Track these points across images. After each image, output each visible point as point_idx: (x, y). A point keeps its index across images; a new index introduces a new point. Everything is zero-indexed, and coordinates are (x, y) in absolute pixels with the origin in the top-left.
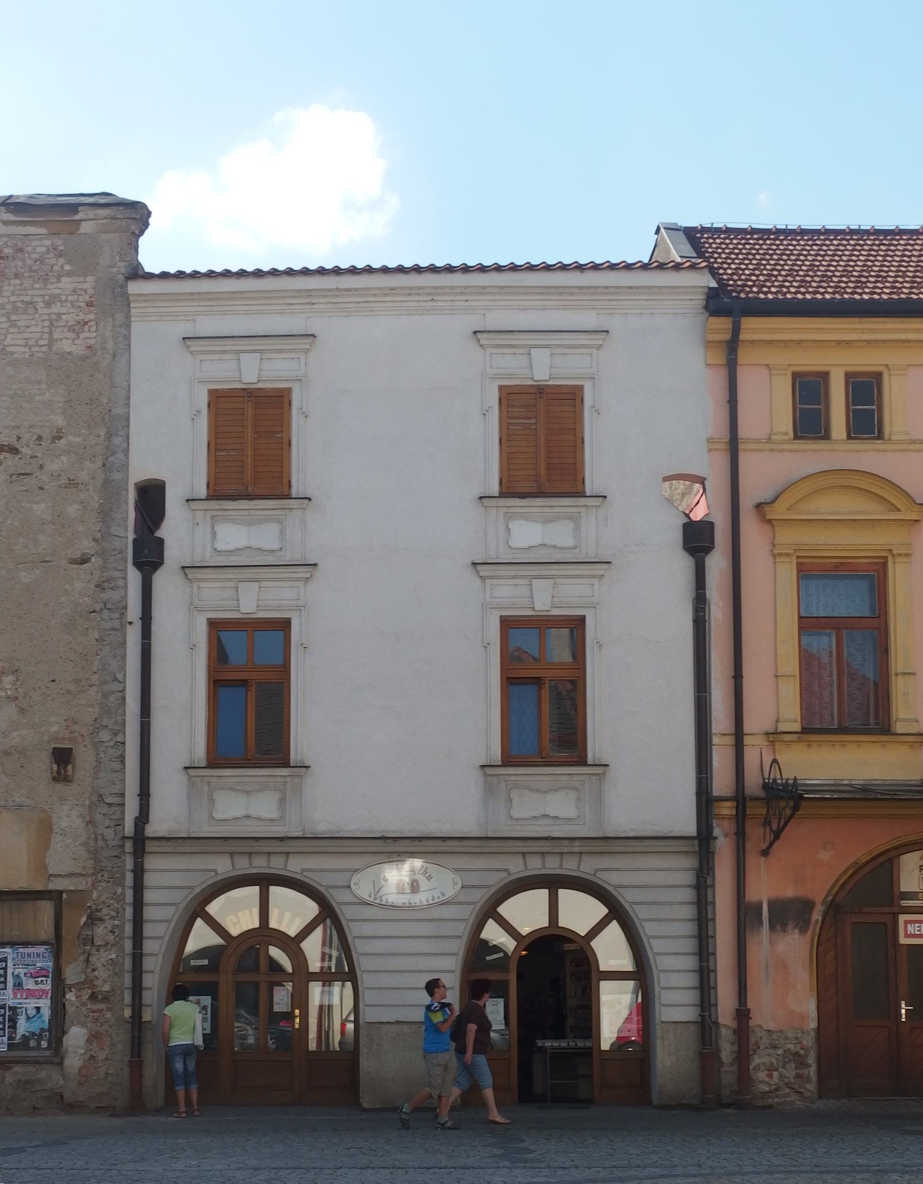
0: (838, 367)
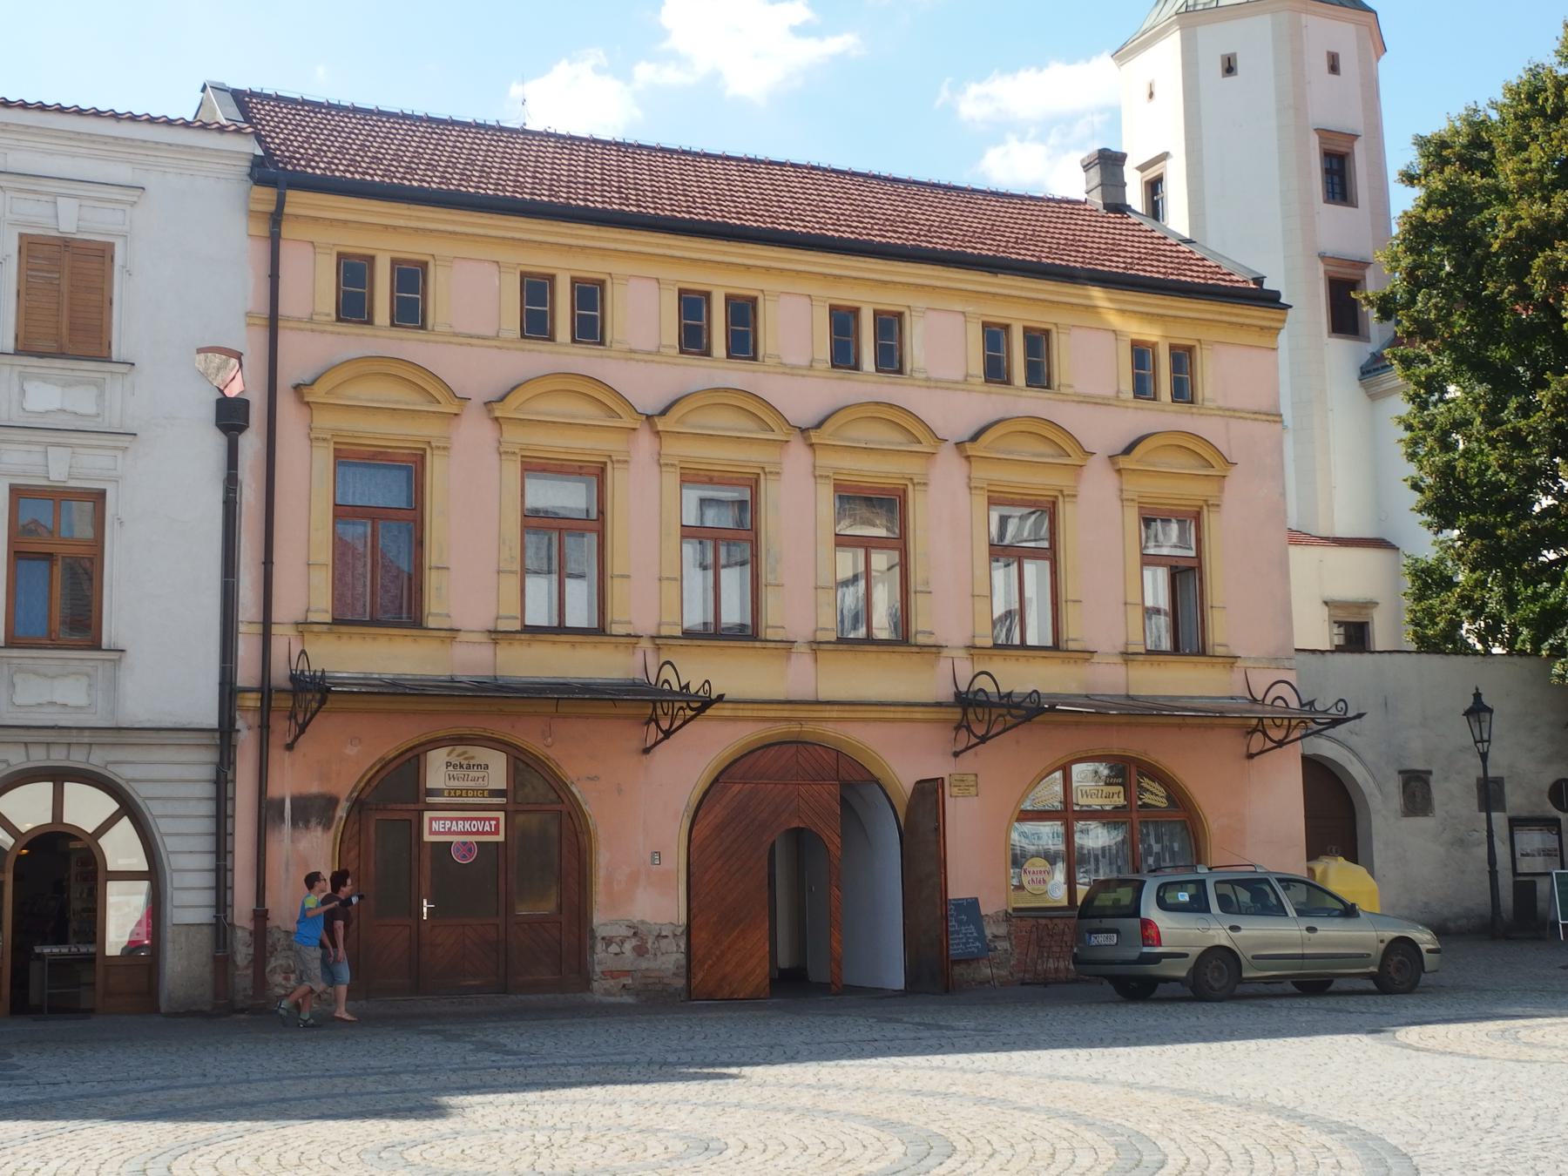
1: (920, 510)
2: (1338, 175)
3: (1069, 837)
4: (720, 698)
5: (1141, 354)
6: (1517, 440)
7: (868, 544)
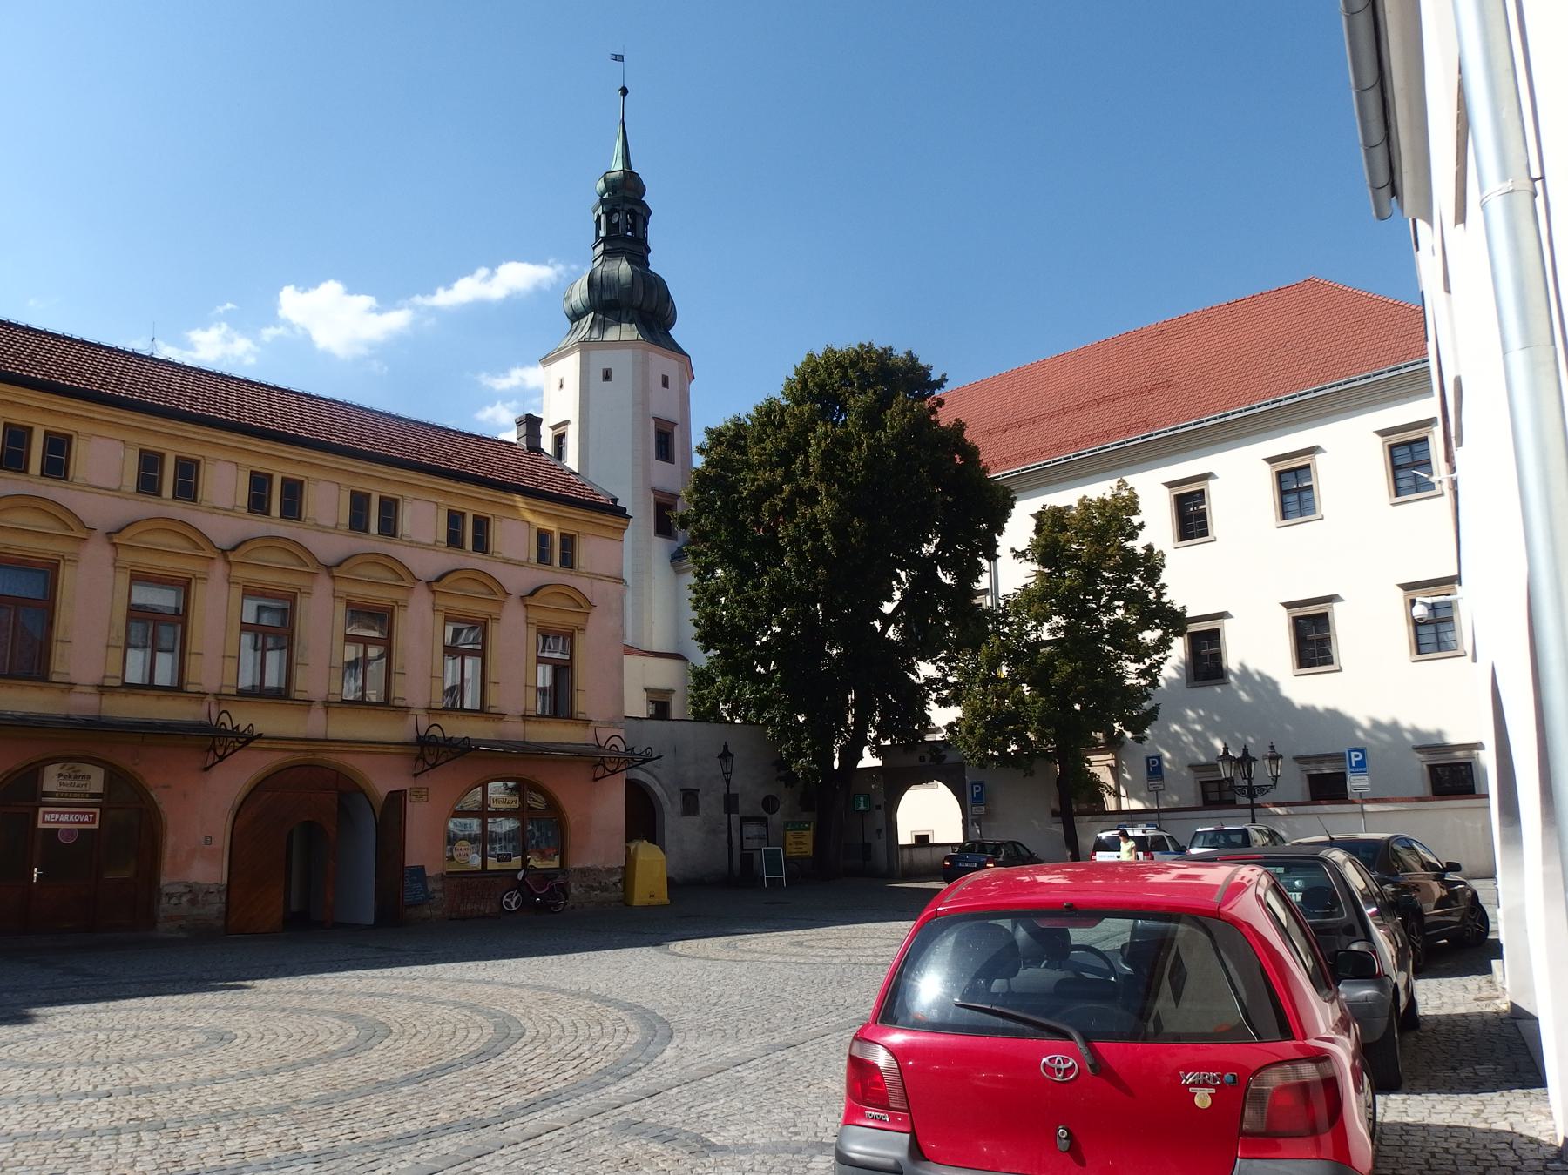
0: (471, 510)
1: (496, 633)
2: (665, 441)
3: (484, 826)
4: (260, 736)
5: (543, 536)
6: (752, 604)
7: (367, 642)
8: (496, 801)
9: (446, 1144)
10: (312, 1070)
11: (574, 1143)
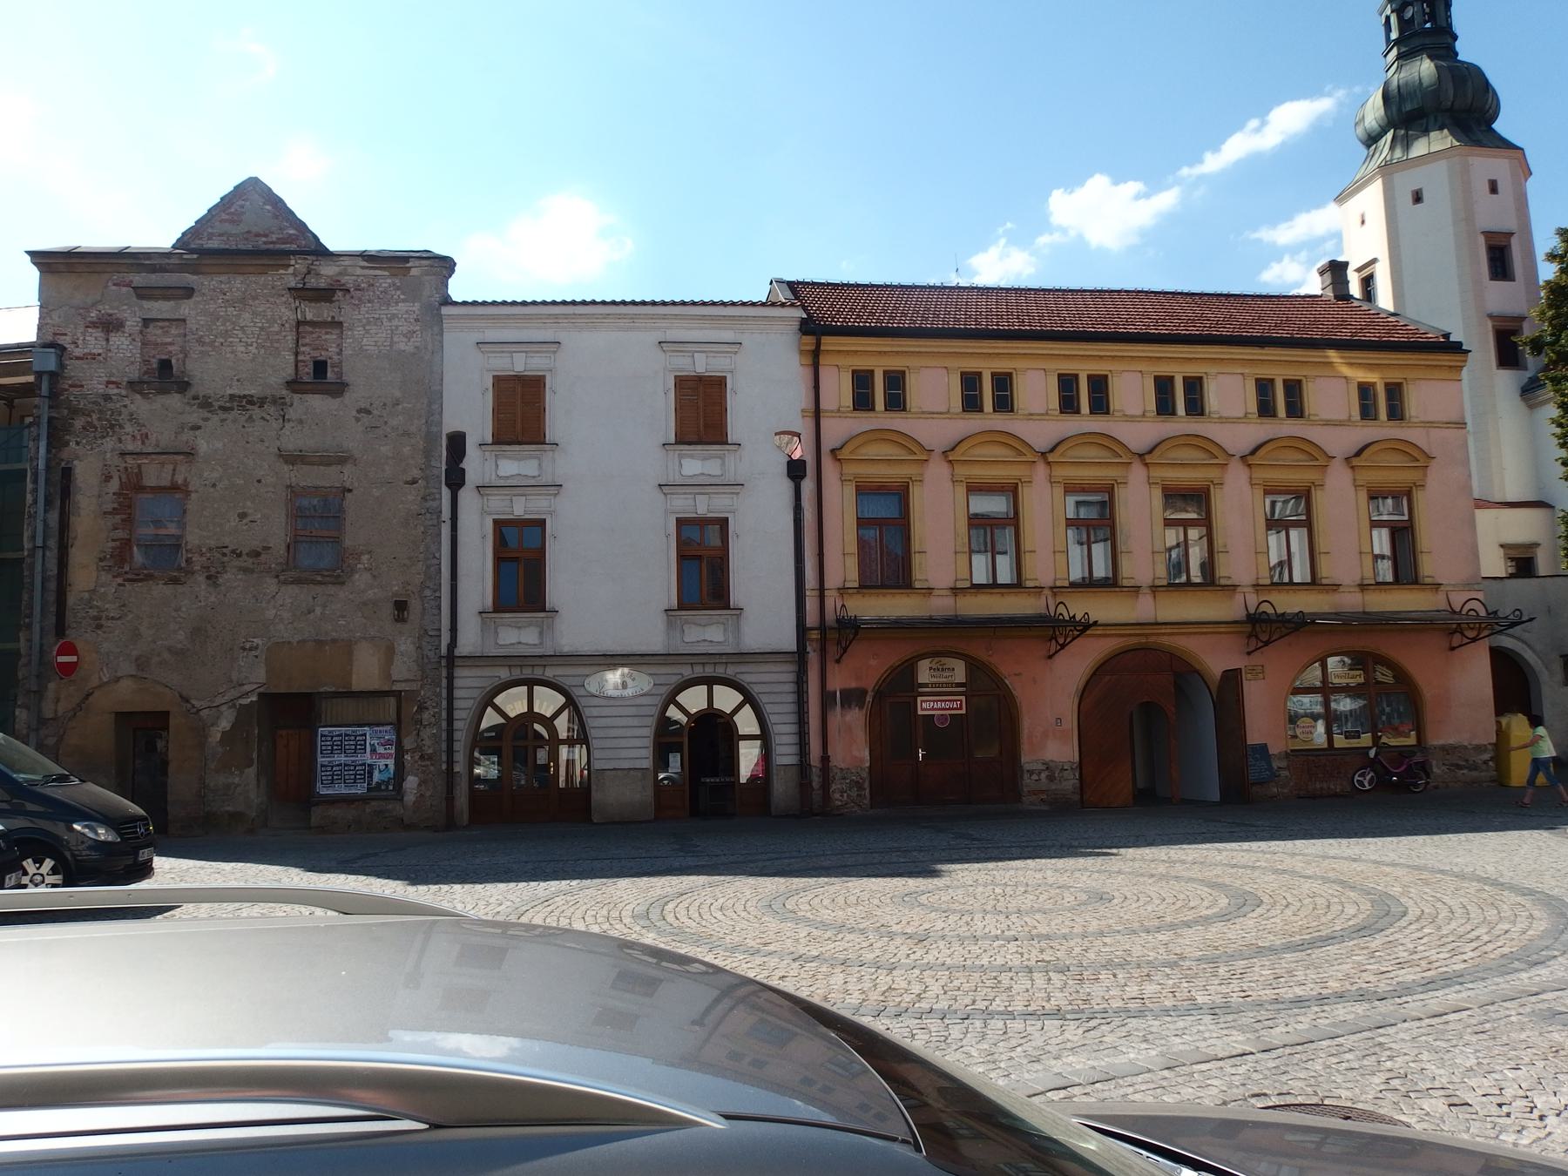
2: (1500, 257)
3: (1326, 704)
7: (1186, 524)
8: (1337, 676)
9: (1342, 1012)
10: (1191, 931)
11: (1488, 1026)
